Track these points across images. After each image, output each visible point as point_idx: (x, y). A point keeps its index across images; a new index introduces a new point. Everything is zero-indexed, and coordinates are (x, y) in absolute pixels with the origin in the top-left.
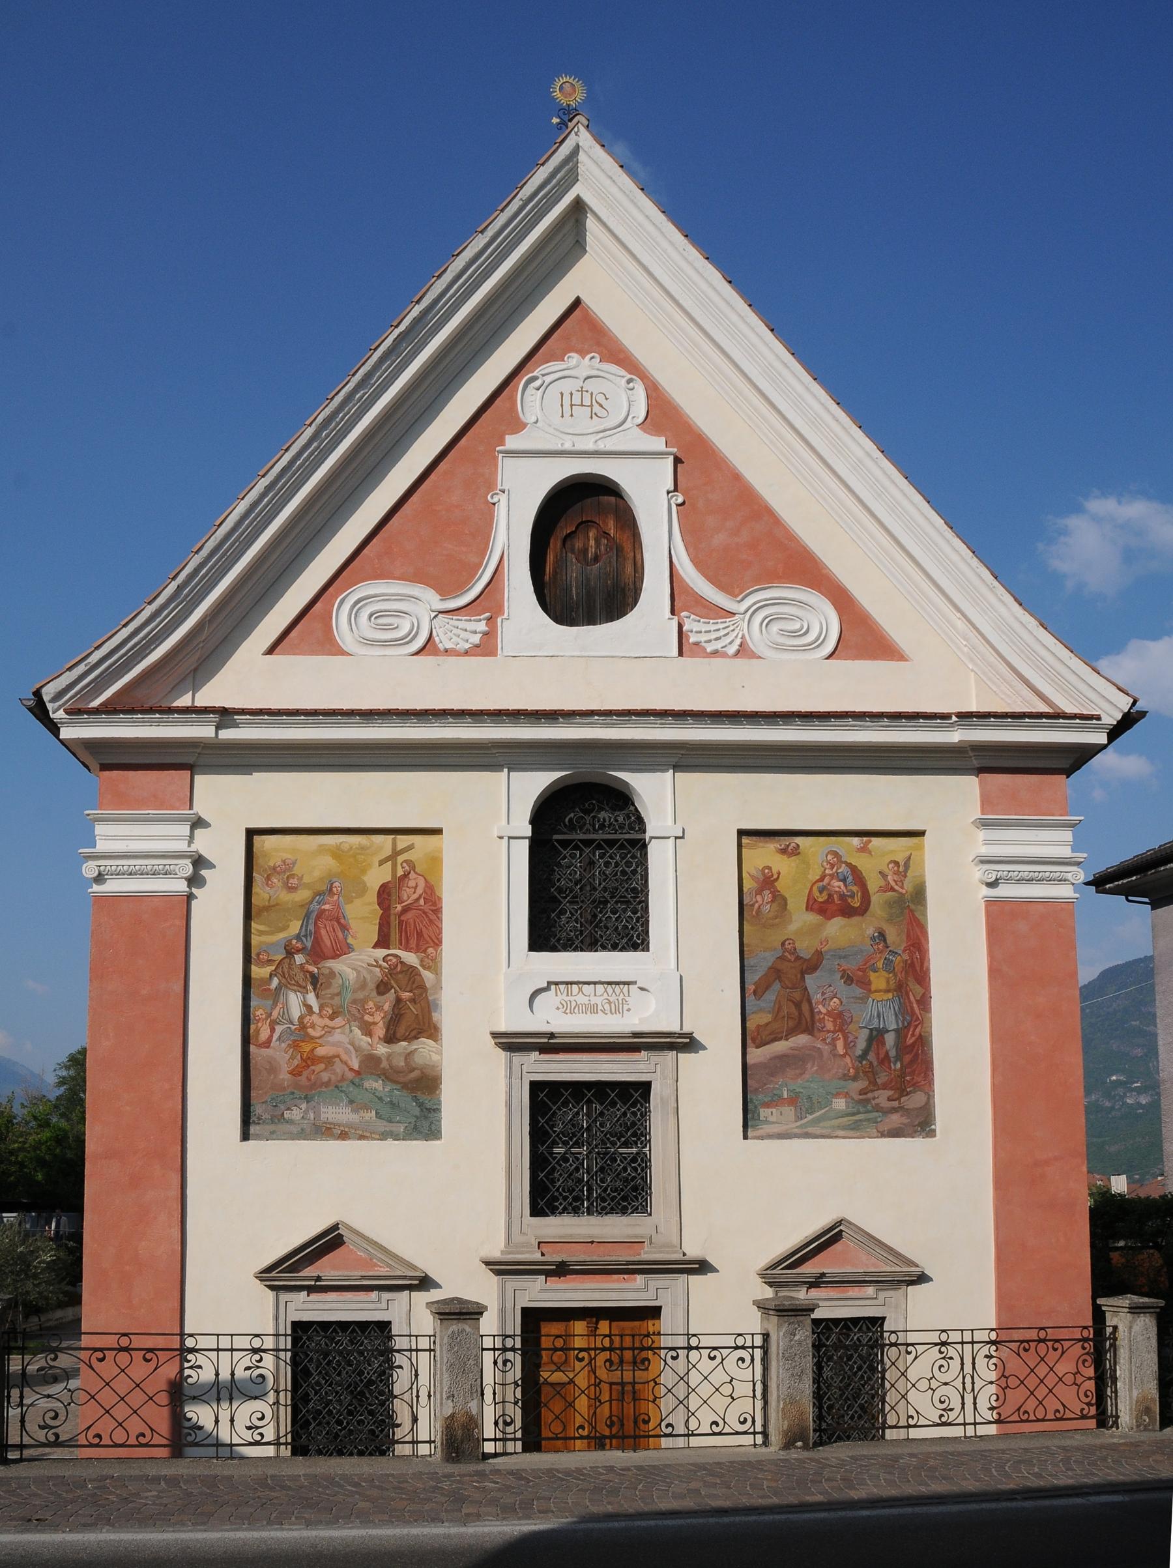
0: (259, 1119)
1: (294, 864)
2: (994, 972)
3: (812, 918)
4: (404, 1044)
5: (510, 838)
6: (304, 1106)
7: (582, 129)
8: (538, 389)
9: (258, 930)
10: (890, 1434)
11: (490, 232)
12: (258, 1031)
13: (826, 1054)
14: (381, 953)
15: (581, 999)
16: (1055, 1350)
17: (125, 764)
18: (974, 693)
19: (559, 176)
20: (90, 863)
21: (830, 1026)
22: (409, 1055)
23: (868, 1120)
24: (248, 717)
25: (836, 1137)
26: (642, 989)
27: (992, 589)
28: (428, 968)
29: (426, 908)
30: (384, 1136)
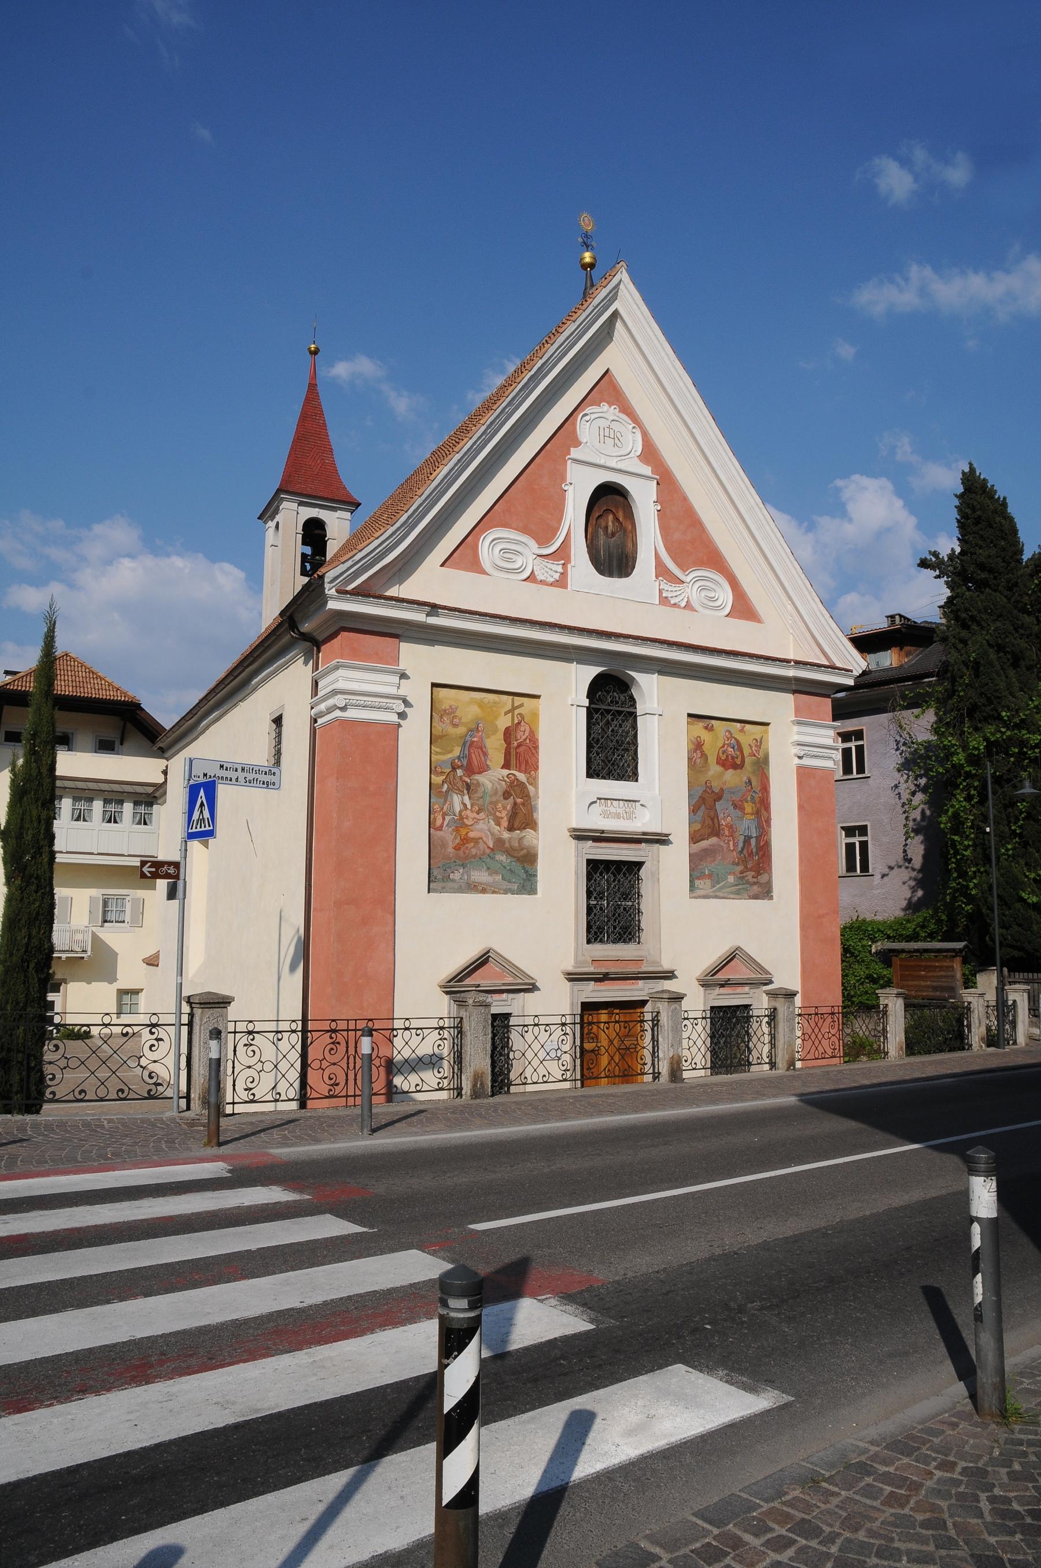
0: (435, 878)
1: (457, 708)
2: (801, 807)
3: (719, 769)
4: (518, 832)
5: (578, 706)
6: (461, 871)
7: (624, 270)
8: (587, 422)
9: (436, 752)
10: (513, 1089)
11: (577, 323)
12: (435, 819)
13: (725, 849)
14: (506, 772)
15: (612, 810)
16: (418, 1035)
17: (352, 628)
18: (792, 647)
19: (610, 295)
20: (339, 696)
21: (727, 833)
22: (521, 839)
23: (743, 889)
24: (446, 611)
25: (730, 898)
26: (642, 805)
27: (810, 593)
28: (531, 784)
29: (531, 745)
30: (506, 892)
